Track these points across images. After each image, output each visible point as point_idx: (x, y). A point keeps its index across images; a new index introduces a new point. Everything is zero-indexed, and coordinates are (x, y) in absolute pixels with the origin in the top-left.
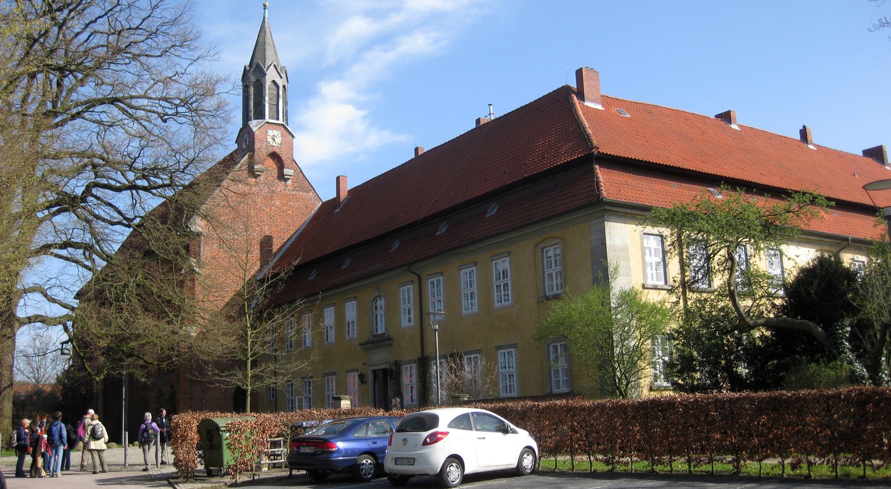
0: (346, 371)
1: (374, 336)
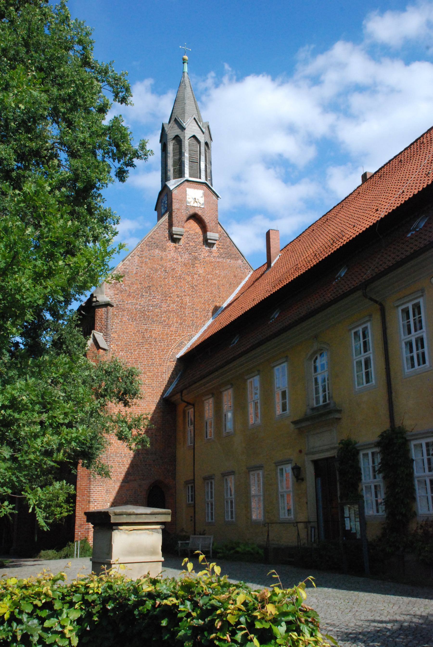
0: (275, 463)
1: (313, 409)
